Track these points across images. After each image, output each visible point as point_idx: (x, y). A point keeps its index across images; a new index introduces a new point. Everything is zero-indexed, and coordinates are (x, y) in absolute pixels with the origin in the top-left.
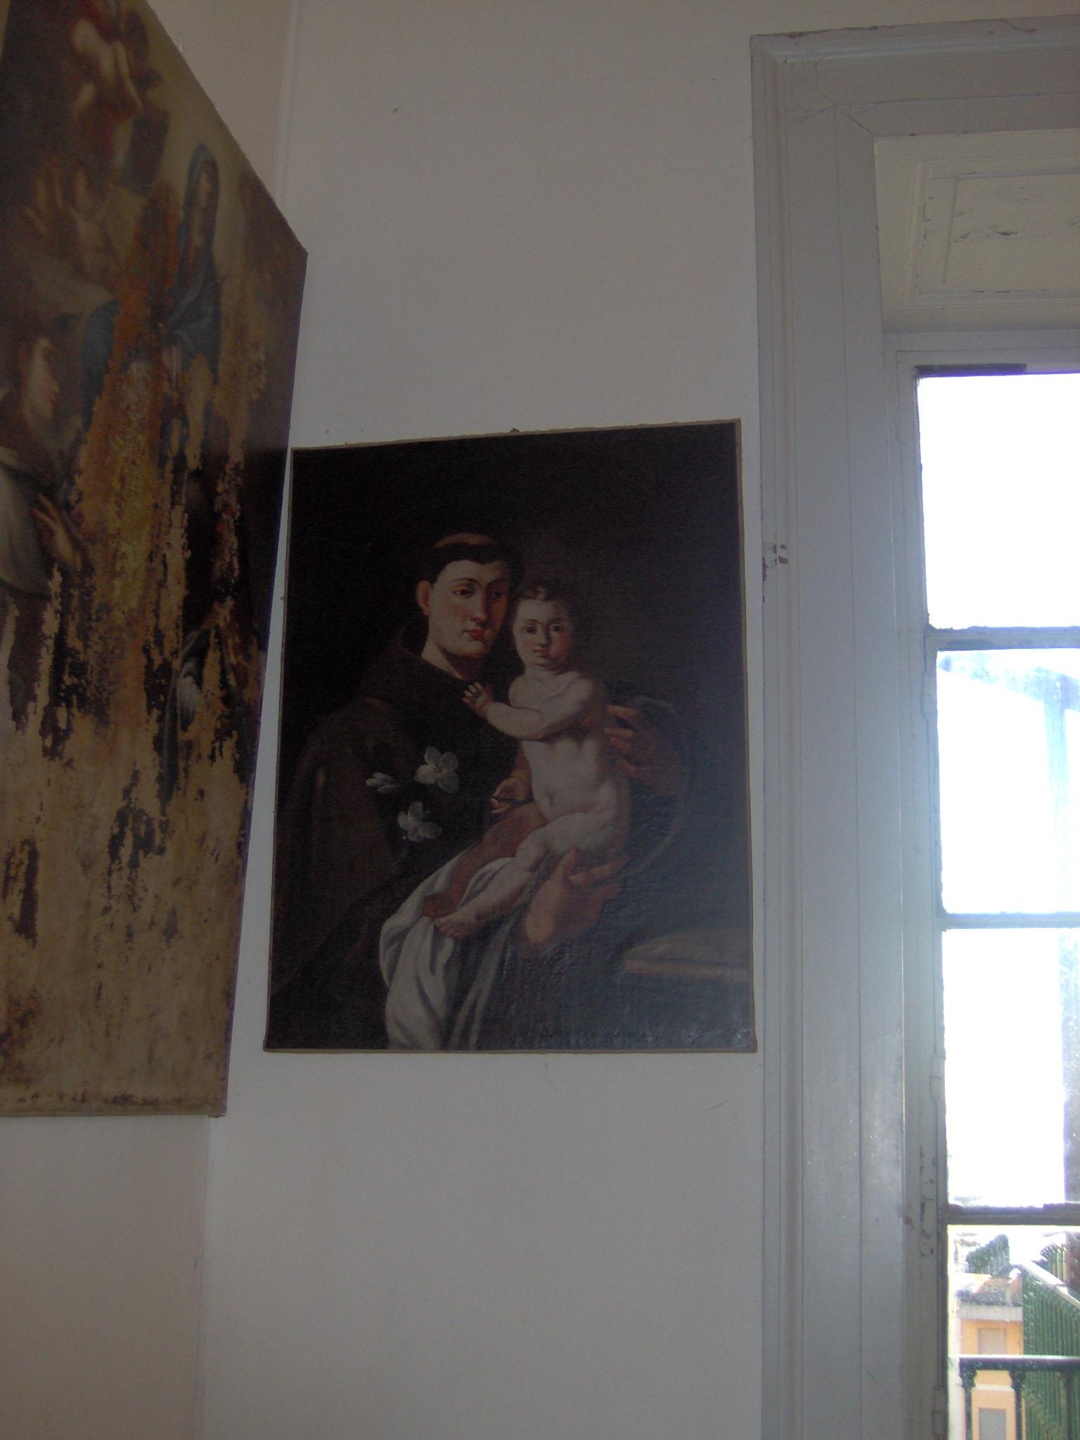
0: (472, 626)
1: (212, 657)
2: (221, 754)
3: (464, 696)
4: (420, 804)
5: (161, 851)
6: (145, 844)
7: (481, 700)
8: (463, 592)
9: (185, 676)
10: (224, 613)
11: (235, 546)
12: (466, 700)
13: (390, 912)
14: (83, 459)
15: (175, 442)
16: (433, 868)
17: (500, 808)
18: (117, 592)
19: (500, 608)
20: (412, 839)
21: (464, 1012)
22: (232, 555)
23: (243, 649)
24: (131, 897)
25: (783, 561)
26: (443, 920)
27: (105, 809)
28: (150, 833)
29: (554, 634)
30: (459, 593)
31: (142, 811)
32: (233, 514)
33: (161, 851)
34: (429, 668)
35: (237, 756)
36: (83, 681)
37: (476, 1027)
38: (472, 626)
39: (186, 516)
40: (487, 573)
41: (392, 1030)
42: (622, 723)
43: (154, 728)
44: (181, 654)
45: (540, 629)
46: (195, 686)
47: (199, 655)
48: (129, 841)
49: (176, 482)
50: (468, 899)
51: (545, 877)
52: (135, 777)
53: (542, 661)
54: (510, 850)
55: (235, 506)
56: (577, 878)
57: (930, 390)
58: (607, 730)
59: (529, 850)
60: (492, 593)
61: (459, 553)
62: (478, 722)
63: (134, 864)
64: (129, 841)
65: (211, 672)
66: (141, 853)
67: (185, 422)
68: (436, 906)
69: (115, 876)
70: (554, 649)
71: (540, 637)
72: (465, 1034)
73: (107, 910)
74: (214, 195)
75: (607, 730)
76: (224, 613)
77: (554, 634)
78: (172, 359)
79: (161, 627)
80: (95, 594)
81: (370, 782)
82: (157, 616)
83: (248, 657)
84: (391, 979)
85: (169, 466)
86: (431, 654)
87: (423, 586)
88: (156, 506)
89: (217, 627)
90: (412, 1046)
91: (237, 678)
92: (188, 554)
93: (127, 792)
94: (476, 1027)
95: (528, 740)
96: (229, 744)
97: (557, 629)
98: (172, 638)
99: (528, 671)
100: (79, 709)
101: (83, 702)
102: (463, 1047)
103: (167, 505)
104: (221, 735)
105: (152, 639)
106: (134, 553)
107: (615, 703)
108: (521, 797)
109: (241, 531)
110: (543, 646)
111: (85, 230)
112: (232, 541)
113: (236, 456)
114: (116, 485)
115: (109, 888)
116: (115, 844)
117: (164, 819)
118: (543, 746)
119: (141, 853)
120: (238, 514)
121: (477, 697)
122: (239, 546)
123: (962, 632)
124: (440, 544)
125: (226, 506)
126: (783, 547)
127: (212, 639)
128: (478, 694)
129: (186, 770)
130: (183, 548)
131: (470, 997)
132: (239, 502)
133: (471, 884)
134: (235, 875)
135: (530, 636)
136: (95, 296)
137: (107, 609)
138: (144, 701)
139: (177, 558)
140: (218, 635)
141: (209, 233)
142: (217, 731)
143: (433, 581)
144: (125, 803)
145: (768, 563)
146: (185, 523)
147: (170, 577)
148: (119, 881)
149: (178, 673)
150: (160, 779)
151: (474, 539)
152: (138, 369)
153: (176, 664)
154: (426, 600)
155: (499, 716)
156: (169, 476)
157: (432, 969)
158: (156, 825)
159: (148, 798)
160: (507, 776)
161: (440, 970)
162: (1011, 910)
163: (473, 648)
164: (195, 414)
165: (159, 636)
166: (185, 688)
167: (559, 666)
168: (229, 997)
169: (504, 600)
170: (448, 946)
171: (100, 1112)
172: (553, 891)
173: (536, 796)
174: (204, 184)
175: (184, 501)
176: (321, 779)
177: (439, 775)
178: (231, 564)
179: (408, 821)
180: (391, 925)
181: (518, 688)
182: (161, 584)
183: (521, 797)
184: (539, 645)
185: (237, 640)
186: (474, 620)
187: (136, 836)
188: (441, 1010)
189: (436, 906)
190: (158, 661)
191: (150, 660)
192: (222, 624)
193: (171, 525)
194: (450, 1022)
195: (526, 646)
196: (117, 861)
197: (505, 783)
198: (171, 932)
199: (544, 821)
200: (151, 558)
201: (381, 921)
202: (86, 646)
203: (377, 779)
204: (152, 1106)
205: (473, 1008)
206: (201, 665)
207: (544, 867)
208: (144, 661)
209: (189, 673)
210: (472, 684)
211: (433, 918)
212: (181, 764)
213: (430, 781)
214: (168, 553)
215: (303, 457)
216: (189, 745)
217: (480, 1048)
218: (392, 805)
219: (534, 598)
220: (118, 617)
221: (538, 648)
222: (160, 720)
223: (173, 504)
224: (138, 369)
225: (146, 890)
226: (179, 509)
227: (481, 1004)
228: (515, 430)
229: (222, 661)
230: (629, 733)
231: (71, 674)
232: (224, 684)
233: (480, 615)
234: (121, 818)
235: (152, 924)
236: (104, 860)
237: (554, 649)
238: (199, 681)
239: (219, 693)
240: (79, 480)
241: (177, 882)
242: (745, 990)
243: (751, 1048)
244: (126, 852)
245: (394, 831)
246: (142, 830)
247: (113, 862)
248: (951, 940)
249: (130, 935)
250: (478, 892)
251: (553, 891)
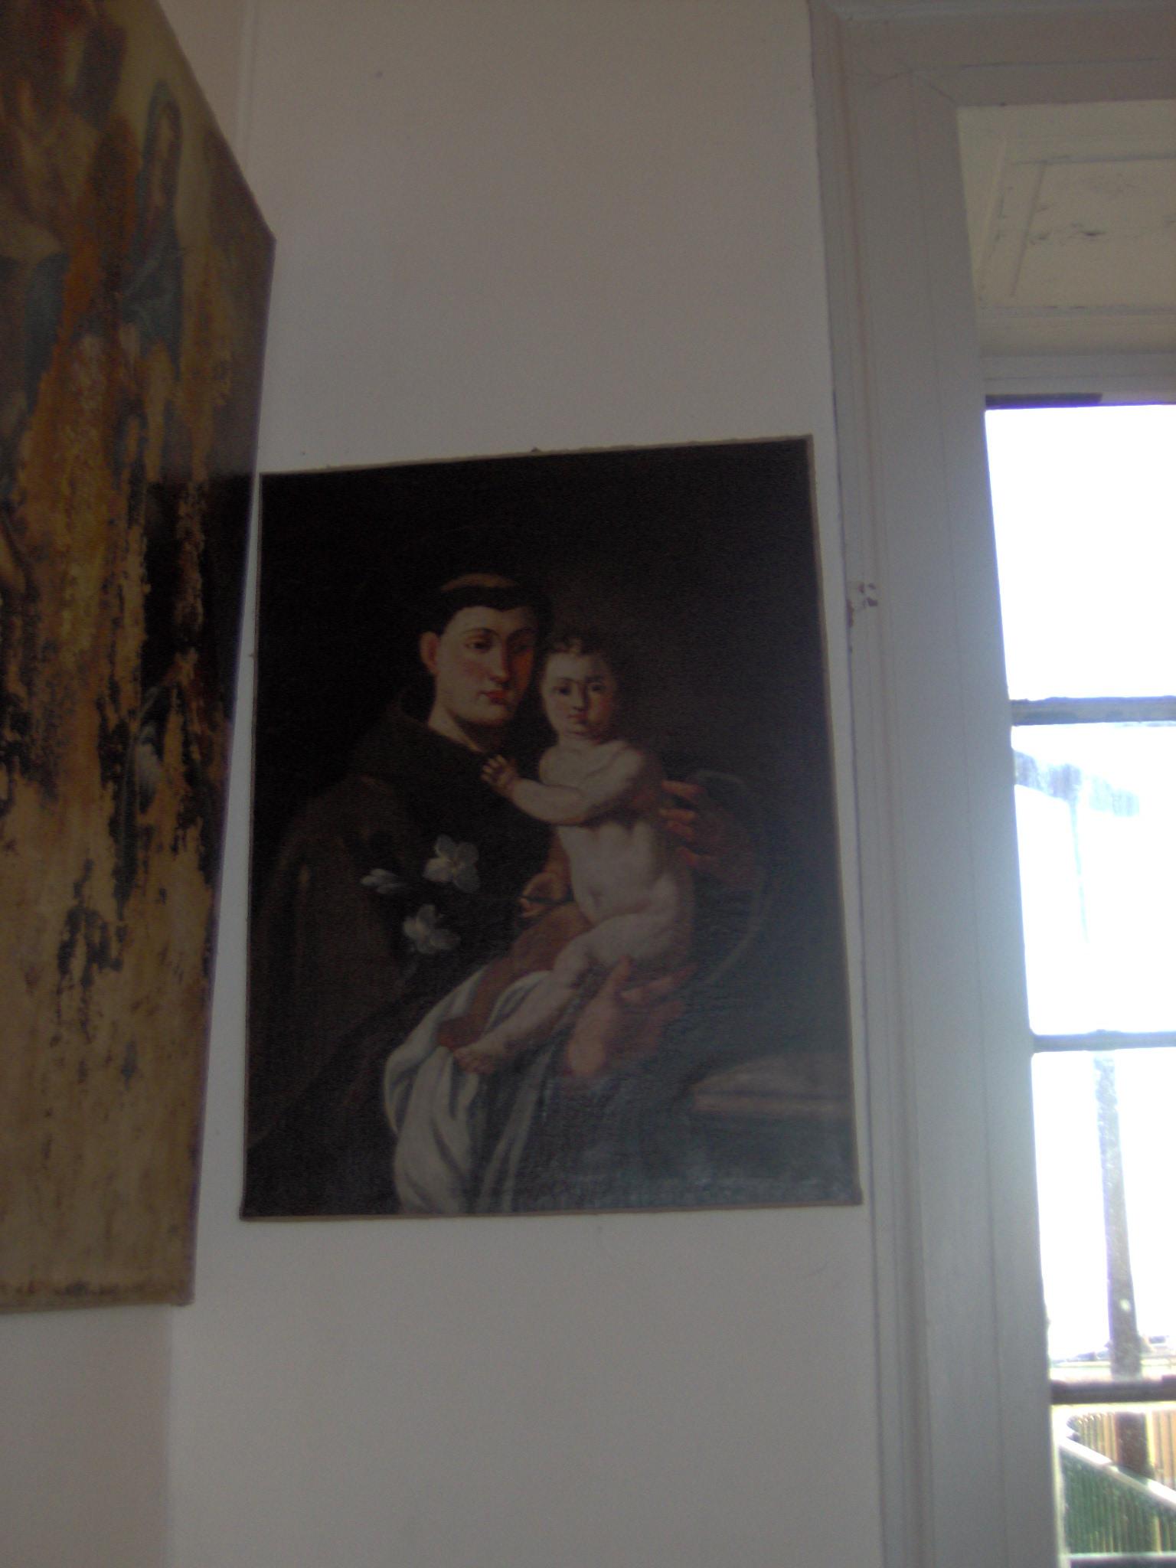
0: (490, 686)
1: (174, 721)
2: (185, 846)
3: (483, 772)
4: (430, 908)
5: (117, 965)
6: (98, 956)
7: (503, 778)
8: (479, 646)
9: (144, 743)
10: (186, 667)
11: (199, 586)
12: (485, 778)
13: (395, 1043)
14: (26, 448)
15: (131, 444)
16: (455, 980)
17: (532, 911)
18: (66, 628)
19: (524, 662)
20: (422, 950)
21: (495, 1164)
22: (196, 597)
23: (207, 716)
24: (84, 1024)
25: (872, 603)
26: (464, 1051)
27: (53, 907)
28: (104, 946)
29: (594, 696)
30: (472, 646)
31: (95, 913)
32: (196, 546)
33: (117, 965)
34: (435, 737)
35: (202, 849)
36: (27, 739)
37: (510, 1184)
38: (490, 686)
39: (145, 540)
40: (506, 622)
41: (403, 1190)
42: (682, 803)
43: (108, 806)
44: (140, 715)
45: (575, 689)
46: (154, 758)
47: (157, 716)
48: (80, 952)
49: (133, 496)
50: (496, 1023)
51: (592, 994)
52: (88, 867)
53: (579, 728)
54: (546, 962)
55: (199, 537)
56: (633, 995)
57: (997, 421)
58: (663, 812)
59: (570, 960)
60: (514, 647)
61: (473, 598)
62: (501, 805)
63: (87, 981)
64: (80, 952)
65: (173, 741)
66: (95, 966)
67: (144, 424)
68: (453, 1034)
69: (65, 996)
70: (593, 715)
71: (575, 700)
72: (496, 1193)
73: (56, 1040)
74: (175, 147)
75: (663, 812)
76: (186, 667)
77: (594, 696)
78: (130, 339)
79: (117, 678)
80: (40, 625)
81: (367, 881)
82: (112, 662)
83: (214, 727)
84: (399, 1127)
85: (126, 475)
86: (440, 721)
87: (428, 638)
88: (111, 522)
89: (179, 686)
90: (428, 1209)
91: (201, 754)
92: (147, 588)
93: (78, 888)
94: (510, 1184)
95: (562, 825)
96: (193, 833)
97: (596, 689)
98: (129, 690)
99: (563, 741)
100: (23, 773)
101: (26, 767)
102: (493, 1210)
103: (122, 524)
104: (184, 821)
105: (107, 692)
106: (85, 577)
107: (670, 778)
108: (557, 894)
109: (205, 568)
110: (580, 710)
111: (30, 156)
112: (194, 579)
113: (201, 475)
114: (65, 490)
115: (59, 1012)
116: (65, 954)
117: (121, 924)
118: (584, 832)
119: (95, 966)
120: (202, 546)
121: (499, 773)
122: (203, 584)
123: (1039, 703)
124: (445, 588)
125: (188, 533)
126: (872, 586)
127: (175, 701)
128: (499, 770)
129: (146, 863)
130: (142, 581)
131: (501, 1147)
132: (206, 532)
133: (499, 1004)
134: (199, 999)
135: (564, 698)
136: (40, 244)
137: (53, 646)
138: (97, 773)
139: (134, 592)
140: (180, 695)
141: (169, 191)
142: (179, 815)
143: (440, 632)
144: (75, 902)
145: (855, 605)
146: (144, 547)
147: (127, 614)
148: (70, 1002)
149: (136, 739)
150: (116, 873)
151: (490, 581)
152: (90, 345)
153: (134, 727)
154: (432, 655)
155: (528, 797)
156: (126, 488)
157: (452, 1110)
158: (112, 930)
159: (102, 896)
160: (540, 870)
161: (462, 1115)
162: (1110, 1026)
163: (493, 713)
164: (155, 416)
165: (114, 689)
166: (143, 755)
167: (601, 734)
168: (194, 1152)
169: (529, 656)
170: (471, 1084)
171: (49, 1307)
172: (601, 1013)
173: (579, 892)
174: (165, 133)
175: (142, 521)
176: (304, 876)
177: (454, 871)
178: (193, 607)
179: (416, 928)
180: (399, 1058)
181: (550, 762)
182: (117, 623)
183: (557, 894)
184: (575, 708)
185: (202, 703)
186: (493, 679)
187: (89, 945)
188: (465, 1164)
189: (453, 1034)
190: (113, 720)
191: (104, 720)
192: (185, 682)
193: (127, 550)
194: (477, 1178)
195: (558, 710)
196: (68, 976)
197: (538, 879)
198: (129, 1070)
199: (588, 925)
200: (105, 588)
201: (385, 1053)
202: (31, 694)
203: (377, 877)
204: (109, 1296)
205: (506, 1160)
206: (161, 730)
207: (589, 981)
208: (97, 720)
209: (148, 740)
210: (492, 757)
211: (452, 1049)
212: (140, 855)
213: (443, 878)
214: (123, 582)
215: (276, 485)
216: (148, 831)
217: (516, 1210)
218: (397, 908)
219: (566, 652)
220: (68, 659)
221: (574, 712)
222: (116, 797)
223: (131, 521)
224: (90, 345)
225: (101, 1015)
226: (136, 532)
227: (516, 1154)
228: (535, 450)
229: (184, 729)
230: (690, 815)
231: (13, 728)
232: (187, 757)
233: (501, 674)
234: (73, 920)
235: (109, 1059)
236: (50, 977)
237: (593, 715)
238: (159, 751)
239: (182, 769)
240: (22, 476)
241: (135, 1006)
242: (845, 1127)
243: (854, 1198)
244: (78, 964)
245: (399, 944)
246: (97, 938)
247: (63, 978)
248: (1041, 1064)
249: (83, 1073)
250: (508, 1016)
251: (601, 1013)
